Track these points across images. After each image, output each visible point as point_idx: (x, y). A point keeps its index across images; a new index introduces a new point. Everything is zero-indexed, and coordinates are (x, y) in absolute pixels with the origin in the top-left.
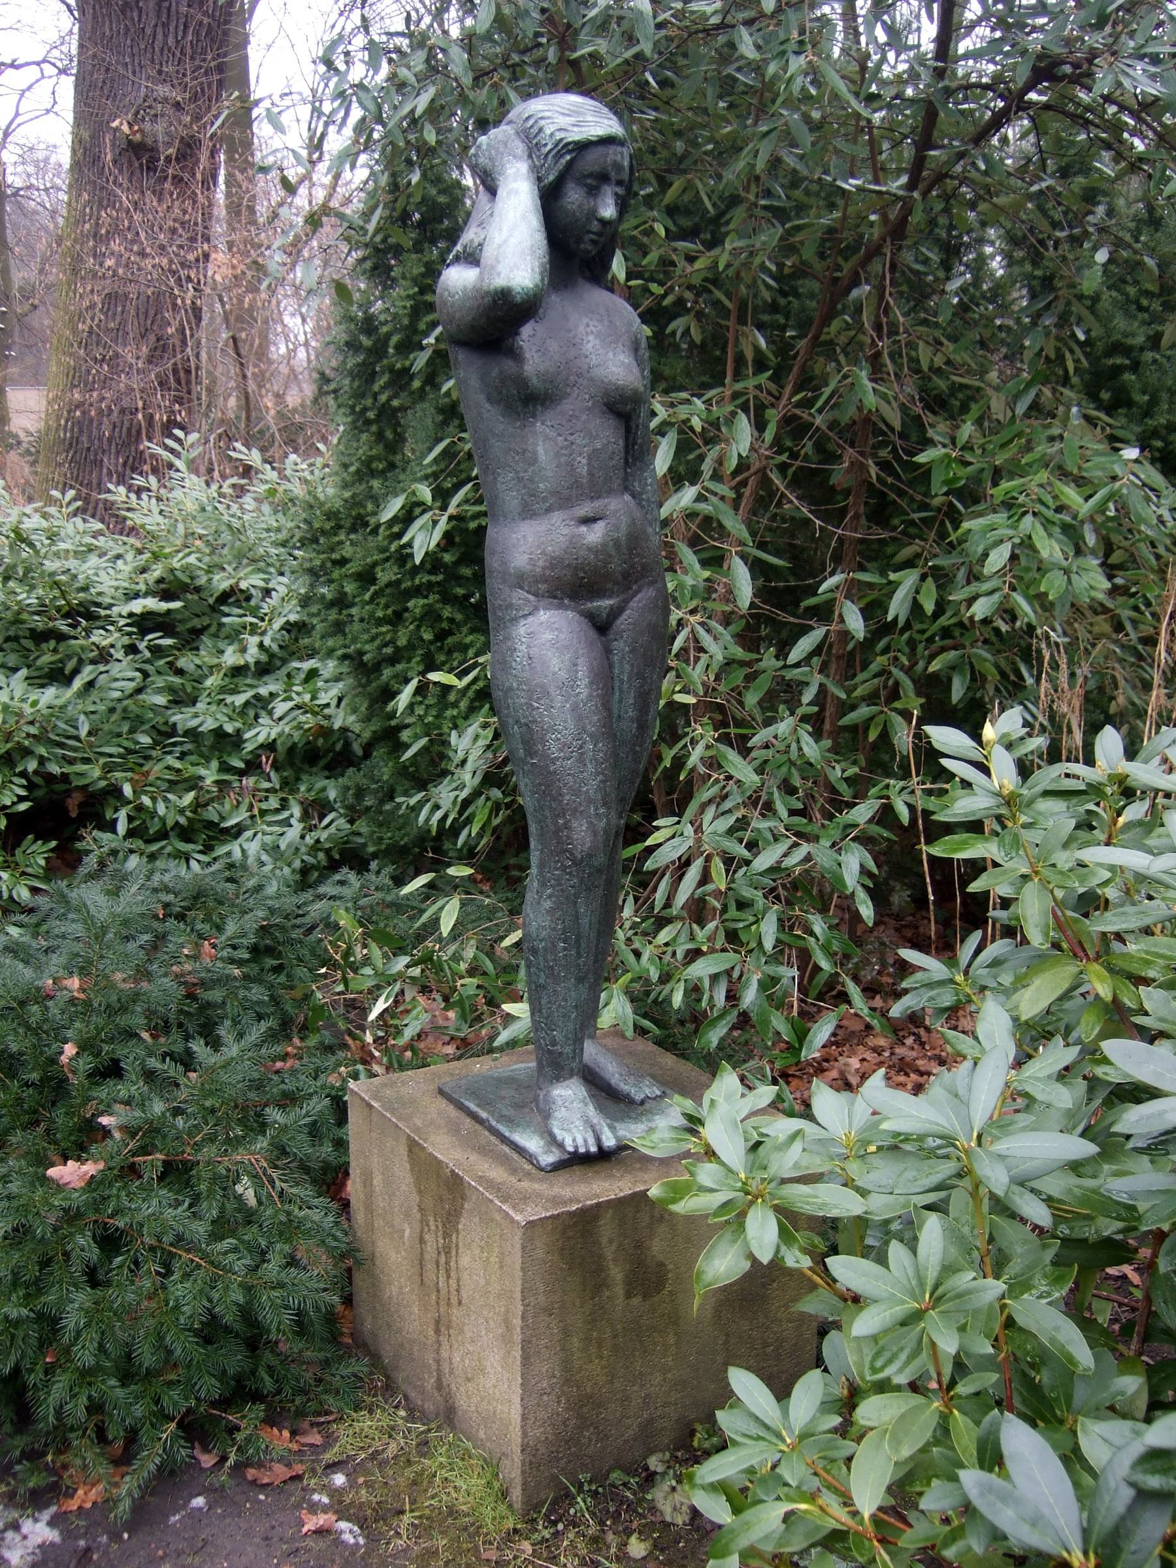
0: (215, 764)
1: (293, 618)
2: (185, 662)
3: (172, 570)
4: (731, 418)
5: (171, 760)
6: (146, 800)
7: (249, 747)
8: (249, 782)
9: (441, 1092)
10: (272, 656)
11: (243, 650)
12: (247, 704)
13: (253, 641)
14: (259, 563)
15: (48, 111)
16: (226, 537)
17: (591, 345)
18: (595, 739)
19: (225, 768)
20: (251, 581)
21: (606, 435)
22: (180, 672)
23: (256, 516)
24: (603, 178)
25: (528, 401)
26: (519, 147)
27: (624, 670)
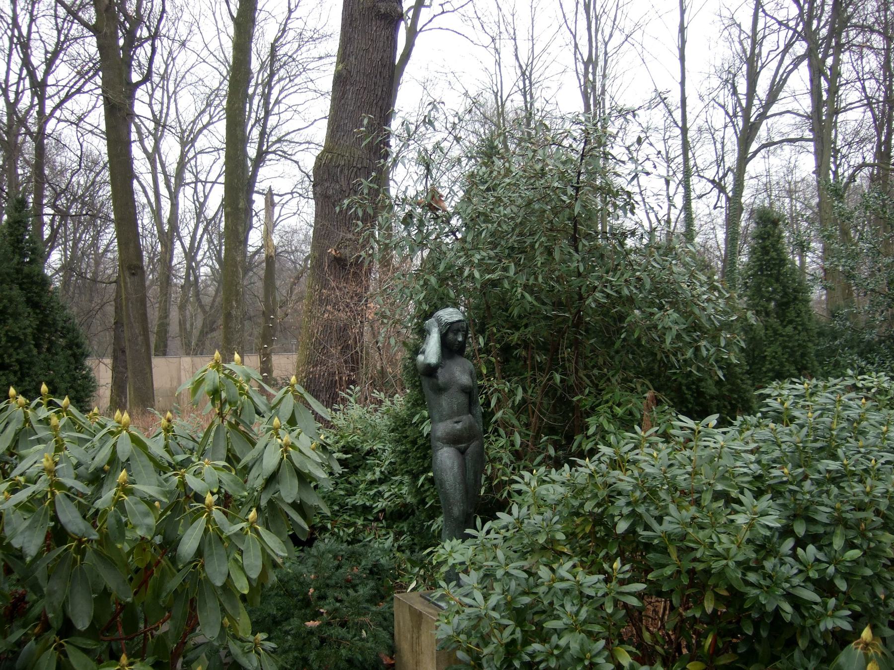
0: (362, 518)
1: (393, 460)
2: (352, 479)
3: (348, 442)
4: (517, 388)
5: (345, 516)
6: (336, 530)
7: (375, 511)
8: (375, 524)
9: (421, 596)
10: (386, 477)
11: (374, 474)
12: (375, 494)
13: (377, 469)
14: (381, 439)
15: (295, 214)
16: (370, 429)
17: (458, 374)
18: (459, 484)
19: (365, 519)
20: (378, 446)
21: (462, 399)
22: (350, 483)
23: (381, 421)
24: (458, 330)
25: (440, 390)
26: (436, 324)
27: (469, 465)
